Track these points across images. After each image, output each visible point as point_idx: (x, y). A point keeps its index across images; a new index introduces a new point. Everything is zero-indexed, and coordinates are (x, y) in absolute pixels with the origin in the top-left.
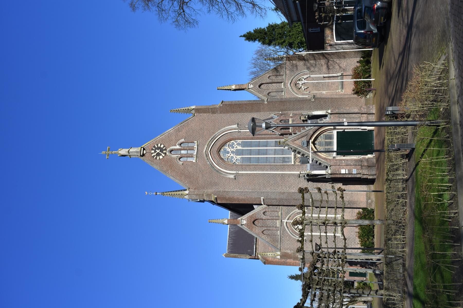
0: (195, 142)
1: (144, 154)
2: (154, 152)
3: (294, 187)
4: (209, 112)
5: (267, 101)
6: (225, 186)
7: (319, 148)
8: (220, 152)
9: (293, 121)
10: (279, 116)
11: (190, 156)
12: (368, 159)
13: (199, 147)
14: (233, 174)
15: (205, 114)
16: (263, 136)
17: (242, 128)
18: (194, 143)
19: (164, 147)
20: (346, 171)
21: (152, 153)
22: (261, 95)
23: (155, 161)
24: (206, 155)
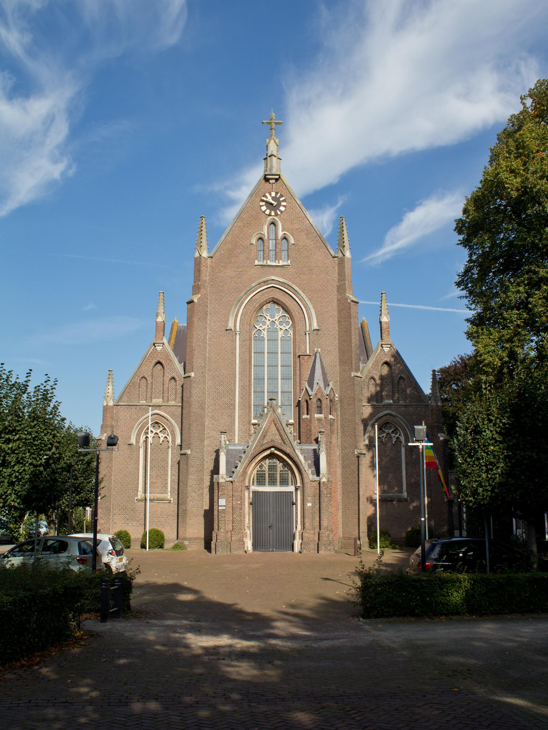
0: (289, 261)
1: (269, 182)
2: (272, 196)
3: (213, 424)
4: (339, 280)
5: (355, 376)
6: (215, 314)
7: (265, 464)
8: (272, 302)
9: (319, 420)
10: (327, 397)
11: (265, 256)
12: (243, 541)
13: (279, 269)
14: (235, 326)
15: (336, 275)
16: (298, 372)
17: (311, 337)
18: (264, 260)
19: (282, 212)
20: (222, 506)
21: (270, 194)
22: (371, 365)
23: (258, 199)
24: (267, 281)
